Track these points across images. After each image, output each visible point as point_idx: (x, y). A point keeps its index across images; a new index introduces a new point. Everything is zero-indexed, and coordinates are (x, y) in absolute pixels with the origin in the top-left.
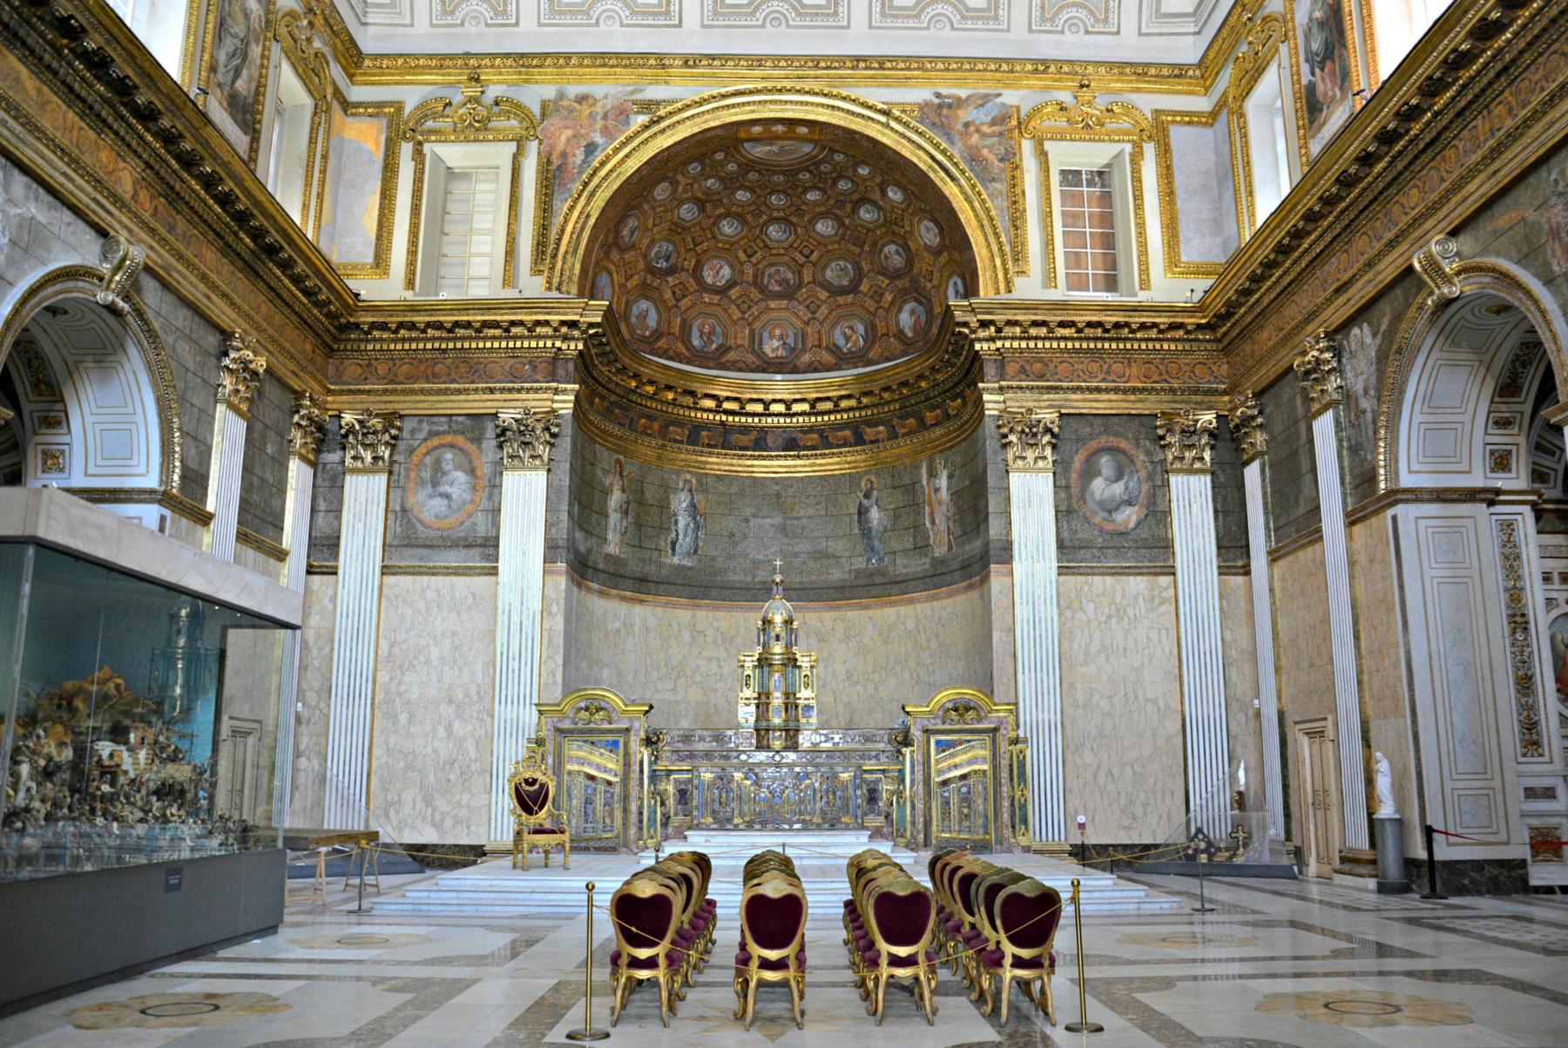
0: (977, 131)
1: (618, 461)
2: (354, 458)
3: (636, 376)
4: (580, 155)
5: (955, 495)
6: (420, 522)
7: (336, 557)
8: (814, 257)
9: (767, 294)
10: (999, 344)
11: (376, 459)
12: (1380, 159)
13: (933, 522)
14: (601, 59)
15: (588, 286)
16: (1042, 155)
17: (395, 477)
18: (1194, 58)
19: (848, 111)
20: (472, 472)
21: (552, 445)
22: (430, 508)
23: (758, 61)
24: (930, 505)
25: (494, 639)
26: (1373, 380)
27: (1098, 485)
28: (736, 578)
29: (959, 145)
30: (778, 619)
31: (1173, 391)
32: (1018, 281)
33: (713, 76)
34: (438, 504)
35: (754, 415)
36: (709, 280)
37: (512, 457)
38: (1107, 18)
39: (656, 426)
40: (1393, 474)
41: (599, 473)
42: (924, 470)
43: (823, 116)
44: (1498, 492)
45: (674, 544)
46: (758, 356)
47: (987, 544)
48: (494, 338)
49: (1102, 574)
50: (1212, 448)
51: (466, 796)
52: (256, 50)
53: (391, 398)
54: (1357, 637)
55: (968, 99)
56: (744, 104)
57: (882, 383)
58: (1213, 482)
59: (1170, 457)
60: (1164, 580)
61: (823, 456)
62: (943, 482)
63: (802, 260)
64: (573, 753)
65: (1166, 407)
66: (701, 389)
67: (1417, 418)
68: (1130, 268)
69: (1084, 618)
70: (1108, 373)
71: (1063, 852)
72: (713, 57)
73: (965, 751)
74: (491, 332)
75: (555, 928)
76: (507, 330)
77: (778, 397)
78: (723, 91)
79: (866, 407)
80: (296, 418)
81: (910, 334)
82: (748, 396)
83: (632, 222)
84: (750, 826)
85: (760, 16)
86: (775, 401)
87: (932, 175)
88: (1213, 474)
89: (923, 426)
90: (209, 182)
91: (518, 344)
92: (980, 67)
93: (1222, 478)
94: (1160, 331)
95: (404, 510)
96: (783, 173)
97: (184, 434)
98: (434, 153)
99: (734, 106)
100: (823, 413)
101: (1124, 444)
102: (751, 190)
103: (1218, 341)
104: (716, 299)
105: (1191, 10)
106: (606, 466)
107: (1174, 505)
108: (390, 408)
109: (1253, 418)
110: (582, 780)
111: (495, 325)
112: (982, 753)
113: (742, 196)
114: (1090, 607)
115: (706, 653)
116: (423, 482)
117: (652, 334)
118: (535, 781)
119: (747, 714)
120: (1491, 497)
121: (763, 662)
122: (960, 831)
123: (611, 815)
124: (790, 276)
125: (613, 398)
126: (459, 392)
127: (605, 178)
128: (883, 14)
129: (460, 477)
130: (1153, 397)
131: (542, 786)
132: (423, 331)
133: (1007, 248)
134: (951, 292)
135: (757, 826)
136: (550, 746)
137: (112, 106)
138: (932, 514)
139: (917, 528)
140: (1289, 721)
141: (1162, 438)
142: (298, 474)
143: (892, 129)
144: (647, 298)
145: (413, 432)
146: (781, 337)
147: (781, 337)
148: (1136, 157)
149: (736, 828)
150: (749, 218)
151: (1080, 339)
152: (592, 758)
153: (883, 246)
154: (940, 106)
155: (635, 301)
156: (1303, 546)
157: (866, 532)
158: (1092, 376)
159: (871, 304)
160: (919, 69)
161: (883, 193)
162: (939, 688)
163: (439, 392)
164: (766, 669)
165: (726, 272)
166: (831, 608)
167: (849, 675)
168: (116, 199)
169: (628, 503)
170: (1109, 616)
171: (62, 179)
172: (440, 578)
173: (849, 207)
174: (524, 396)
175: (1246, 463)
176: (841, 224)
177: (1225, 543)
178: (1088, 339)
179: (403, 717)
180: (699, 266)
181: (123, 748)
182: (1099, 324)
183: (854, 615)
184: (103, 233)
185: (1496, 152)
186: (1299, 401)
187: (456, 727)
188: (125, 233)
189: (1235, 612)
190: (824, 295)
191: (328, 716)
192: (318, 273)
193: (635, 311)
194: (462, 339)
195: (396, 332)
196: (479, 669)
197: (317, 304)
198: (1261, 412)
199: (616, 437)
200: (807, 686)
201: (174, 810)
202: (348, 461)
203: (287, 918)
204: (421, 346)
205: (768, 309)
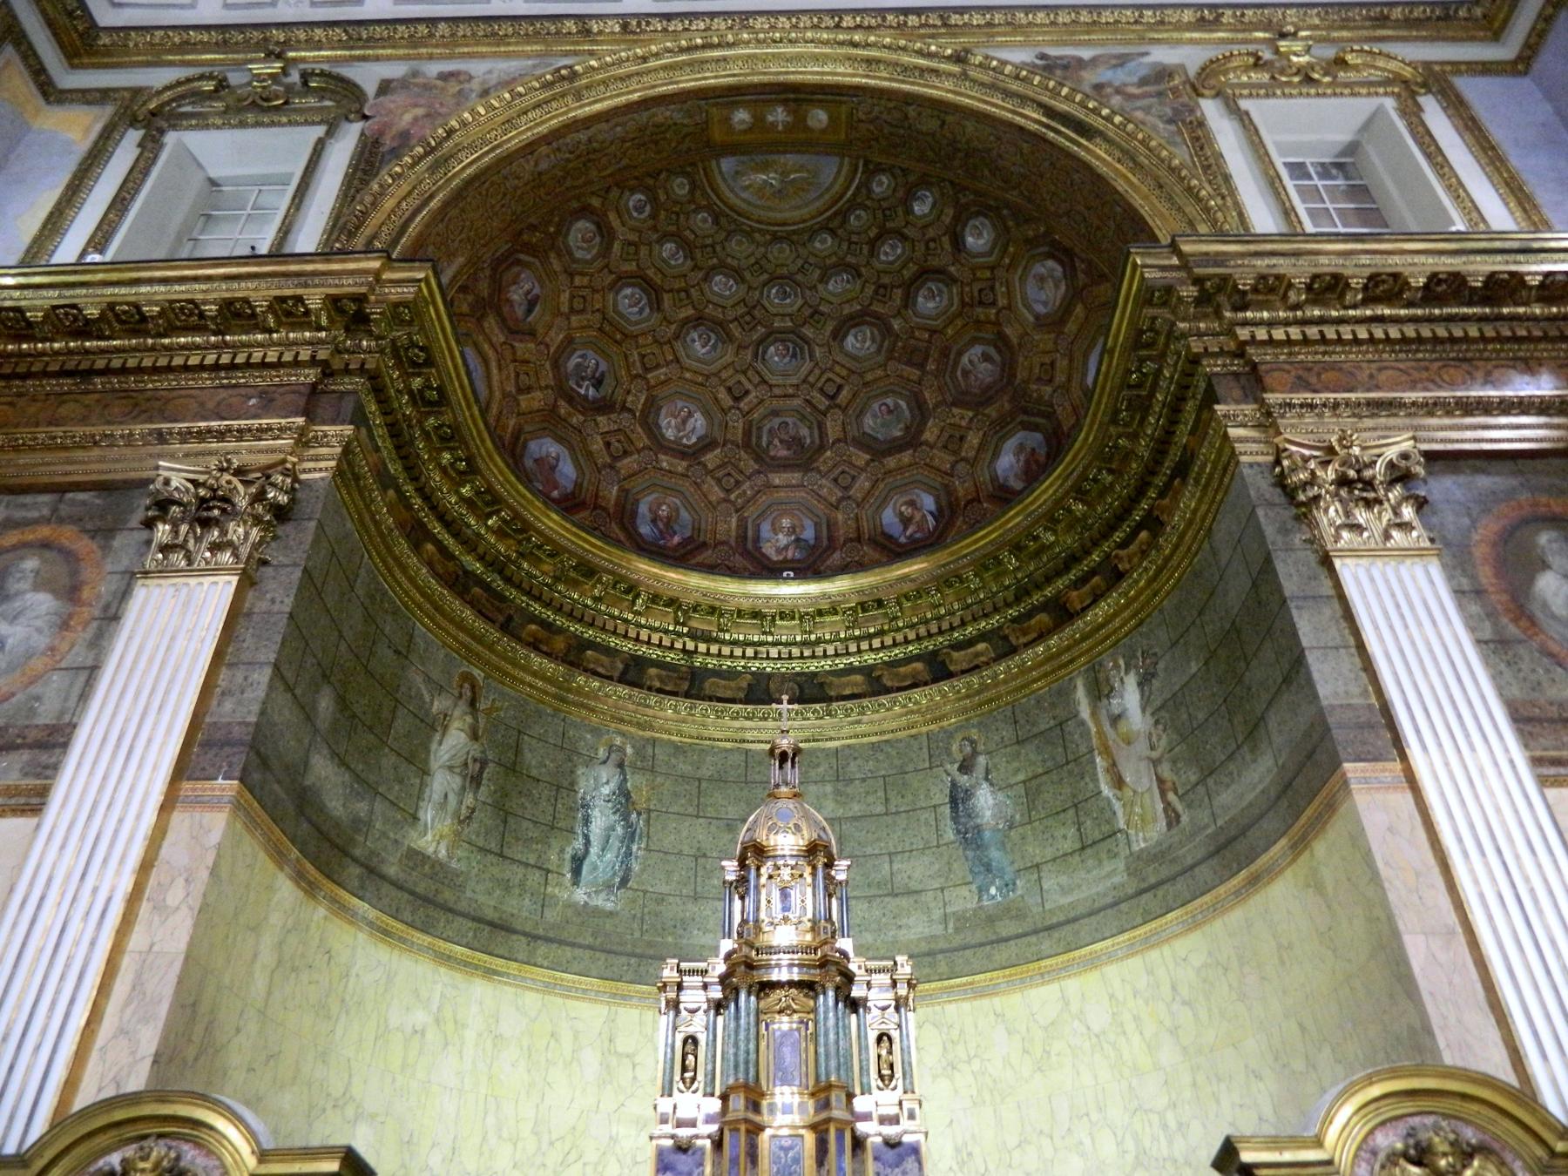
1: (467, 678)
13: (1119, 783)
24: (1106, 751)
36: (670, 434)
42: (1081, 694)
45: (578, 863)
62: (1129, 697)
63: (823, 403)
98: (180, 145)
104: (681, 466)
106: (436, 674)
124: (804, 432)
153: (960, 354)
157: (971, 837)
159: (943, 460)
165: (698, 422)
176: (887, 330)
180: (652, 406)
190: (862, 458)
205: (769, 486)
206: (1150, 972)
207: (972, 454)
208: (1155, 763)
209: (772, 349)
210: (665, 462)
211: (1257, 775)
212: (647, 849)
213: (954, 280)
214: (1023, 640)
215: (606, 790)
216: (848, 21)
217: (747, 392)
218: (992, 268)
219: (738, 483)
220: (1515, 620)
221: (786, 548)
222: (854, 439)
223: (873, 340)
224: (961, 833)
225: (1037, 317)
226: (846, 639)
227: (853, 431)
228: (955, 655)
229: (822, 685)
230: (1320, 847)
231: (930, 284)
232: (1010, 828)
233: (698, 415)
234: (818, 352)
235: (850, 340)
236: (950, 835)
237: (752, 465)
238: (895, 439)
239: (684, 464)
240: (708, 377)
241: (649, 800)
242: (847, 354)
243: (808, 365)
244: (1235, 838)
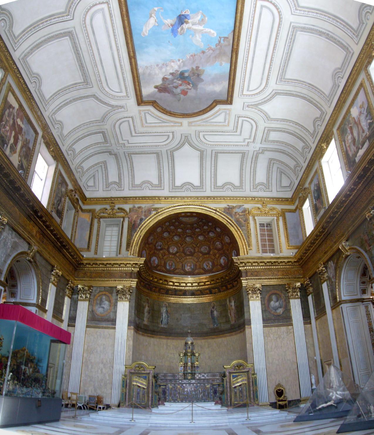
0: (238, 214)
1: (147, 299)
2: (81, 297)
3: (152, 276)
4: (139, 221)
5: (236, 307)
6: (96, 314)
7: (75, 322)
8: (198, 245)
9: (186, 255)
10: (246, 268)
11: (86, 297)
12: (331, 222)
15: (140, 253)
17: (90, 302)
18: (290, 196)
19: (206, 210)
20: (110, 301)
21: (130, 295)
22: (99, 311)
23: (183, 198)
25: (114, 346)
26: (334, 274)
27: (272, 303)
29: (234, 218)
30: (189, 343)
31: (290, 278)
32: (250, 252)
34: (101, 310)
35: (183, 286)
36: (171, 251)
37: (120, 298)
39: (157, 289)
40: (340, 297)
41: (142, 302)
42: (228, 301)
44: (364, 299)
45: (162, 321)
47: (244, 320)
49: (274, 327)
50: (300, 292)
52: (63, 199)
53: (90, 282)
54: (336, 338)
55: (236, 206)
57: (216, 278)
58: (301, 301)
59: (290, 295)
61: (201, 297)
62: (233, 304)
63: (195, 246)
64: (134, 379)
65: (288, 282)
66: (168, 279)
67: (345, 283)
68: (277, 248)
70: (273, 274)
71: (268, 405)
72: (172, 197)
73: (240, 378)
74: (115, 266)
75: (129, 428)
77: (189, 282)
79: (212, 284)
80: (67, 286)
81: (223, 265)
82: (181, 282)
83: (152, 237)
84: (182, 401)
85: (184, 189)
86: (188, 283)
88: (301, 299)
89: (227, 289)
90: (52, 231)
91: (122, 269)
93: (303, 299)
94: (285, 263)
95: (92, 311)
97: (42, 290)
99: (177, 209)
100: (201, 286)
101: (278, 292)
102: (182, 229)
103: (299, 265)
104: (173, 256)
105: (288, 185)
107: (291, 307)
108: (90, 285)
109: (309, 284)
110: (136, 387)
111: (117, 264)
112: (245, 378)
113: (179, 230)
116: (97, 304)
117: (157, 265)
119: (181, 369)
120: (362, 300)
121: (185, 354)
122: (240, 401)
123: (144, 397)
124: (192, 250)
125: (146, 282)
126: (107, 281)
127: (145, 227)
128: (214, 188)
129: (107, 303)
130: (285, 280)
132: (99, 265)
133: (247, 243)
134: (233, 254)
135: (184, 401)
136: (128, 377)
137: (33, 216)
138: (230, 312)
139: (227, 316)
140: (323, 362)
141: (288, 290)
142: (67, 300)
144: (155, 256)
145: (95, 291)
146: (190, 266)
148: (278, 220)
149: (178, 402)
150: (181, 236)
151: (266, 266)
152: (139, 381)
154: (229, 208)
155: (152, 257)
156: (323, 316)
157: (213, 317)
158: (269, 275)
159: (213, 257)
161: (215, 229)
162: (233, 360)
163: (102, 281)
164: (186, 356)
165: (176, 249)
166: (204, 339)
167: (209, 358)
168: (32, 236)
169: (150, 310)
170: (277, 338)
171: (22, 232)
172: (101, 329)
173: (207, 233)
174: (123, 282)
175: (308, 295)
176: (205, 237)
178: (268, 266)
179: (90, 366)
180: (168, 248)
181: (27, 368)
182: (270, 262)
183: (210, 340)
184: (29, 244)
185: (353, 222)
186: (319, 280)
187: (104, 370)
188: (33, 243)
189: (308, 334)
190: (201, 255)
191: (71, 365)
192: (74, 251)
193: (152, 259)
194: (109, 267)
195: (92, 265)
197: (74, 258)
198: (311, 282)
199: (147, 292)
200: (197, 361)
201: (37, 385)
202: (79, 298)
203: (61, 418)
204: (98, 269)
205: (187, 259)
210: (171, 256)
216: (199, 198)
224: (212, 317)
227: (200, 250)
234: (194, 239)
236: (210, 317)
237: (184, 255)
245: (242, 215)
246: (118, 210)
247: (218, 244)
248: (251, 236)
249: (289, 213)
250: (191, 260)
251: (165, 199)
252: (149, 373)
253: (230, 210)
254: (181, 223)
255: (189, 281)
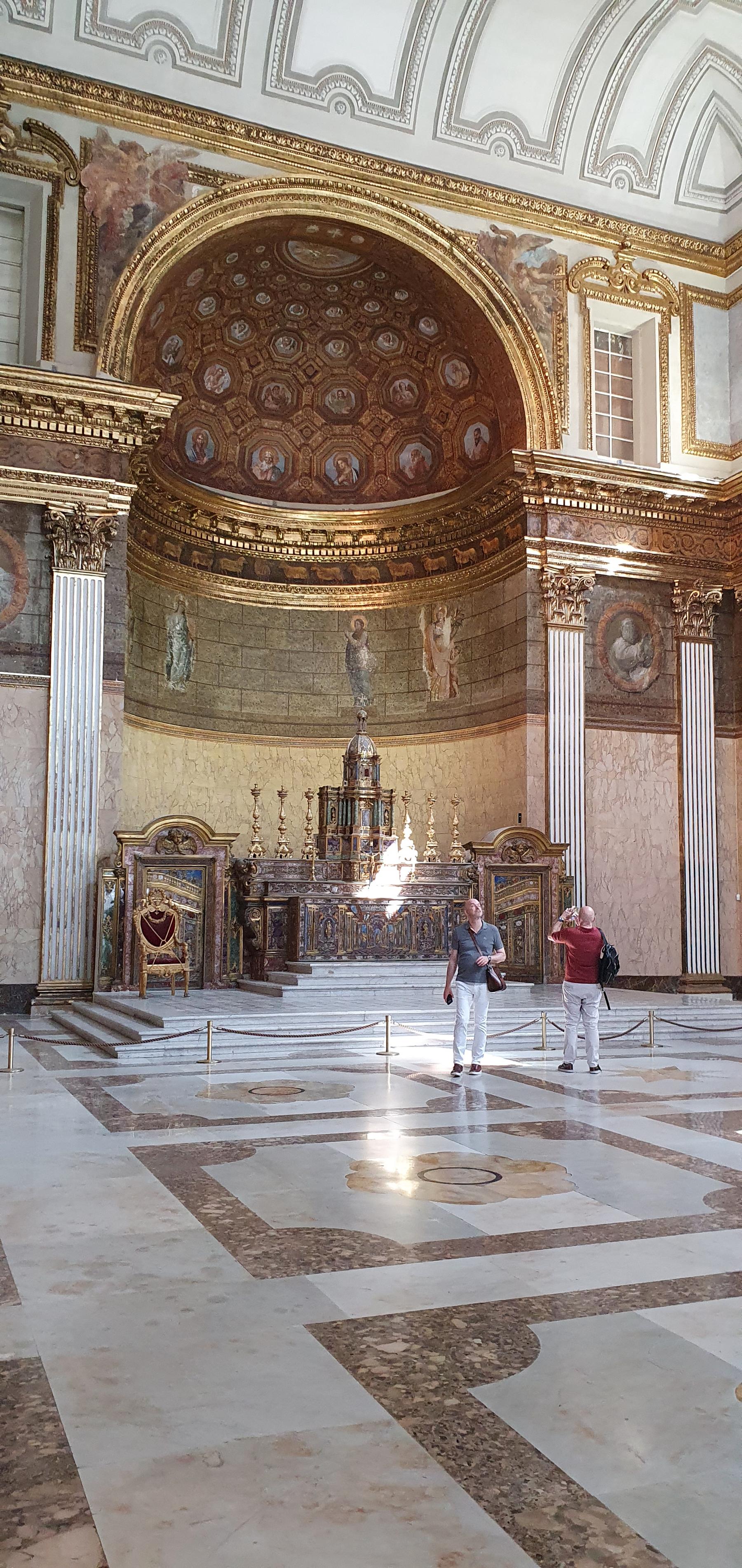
0: (529, 275)
4: (127, 219)
8: (317, 379)
9: (263, 412)
13: (432, 668)
14: (154, 104)
16: (584, 312)
24: (429, 651)
27: (619, 643)
28: (224, 708)
33: (275, 155)
36: (209, 386)
38: (650, 178)
42: (422, 616)
43: (387, 229)
45: (169, 667)
46: (247, 477)
48: (42, 417)
51: (12, 931)
56: (309, 196)
60: (671, 738)
62: (446, 629)
63: (303, 379)
69: (604, 769)
72: (278, 134)
74: (39, 410)
76: (61, 411)
78: (293, 176)
81: (411, 476)
82: (244, 519)
84: (352, 957)
87: (487, 313)
92: (537, 206)
96: (312, 282)
102: (273, 294)
113: (262, 298)
114: (608, 759)
115: (196, 783)
118: (161, 914)
124: (288, 395)
131: (170, 918)
135: (359, 958)
143: (454, 257)
146: (271, 460)
147: (271, 460)
149: (339, 959)
153: (396, 378)
154: (496, 241)
159: (370, 440)
160: (480, 196)
166: (317, 745)
169: (133, 619)
174: (74, 488)
176: (354, 347)
177: (719, 708)
180: (201, 369)
190: (320, 421)
196: (26, 791)
206: (428, 752)
207: (387, 442)
208: (451, 666)
209: (281, 339)
211: (492, 695)
212: (197, 660)
213: (405, 339)
214: (397, 574)
215: (178, 628)
217: (259, 363)
218: (430, 345)
219: (243, 422)
220: (602, 660)
221: (267, 471)
222: (318, 406)
223: (344, 350)
225: (447, 385)
226: (301, 546)
228: (359, 569)
229: (282, 570)
230: (509, 734)
231: (389, 333)
232: (375, 673)
233: (227, 375)
235: (330, 345)
236: (344, 670)
238: (343, 415)
239: (214, 406)
240: (237, 351)
241: (197, 633)
242: (327, 355)
243: (300, 354)
244: (477, 713)
245: (541, 282)
246: (25, 135)
247: (404, 388)
248: (567, 377)
249: (707, 308)
250: (279, 436)
251: (248, 136)
252: (213, 860)
253: (500, 248)
254: (282, 266)
255: (300, 524)
